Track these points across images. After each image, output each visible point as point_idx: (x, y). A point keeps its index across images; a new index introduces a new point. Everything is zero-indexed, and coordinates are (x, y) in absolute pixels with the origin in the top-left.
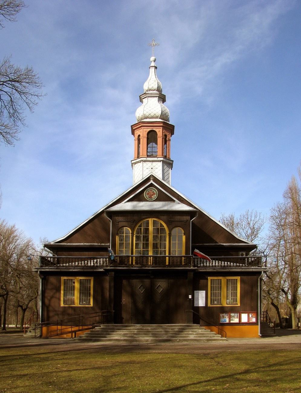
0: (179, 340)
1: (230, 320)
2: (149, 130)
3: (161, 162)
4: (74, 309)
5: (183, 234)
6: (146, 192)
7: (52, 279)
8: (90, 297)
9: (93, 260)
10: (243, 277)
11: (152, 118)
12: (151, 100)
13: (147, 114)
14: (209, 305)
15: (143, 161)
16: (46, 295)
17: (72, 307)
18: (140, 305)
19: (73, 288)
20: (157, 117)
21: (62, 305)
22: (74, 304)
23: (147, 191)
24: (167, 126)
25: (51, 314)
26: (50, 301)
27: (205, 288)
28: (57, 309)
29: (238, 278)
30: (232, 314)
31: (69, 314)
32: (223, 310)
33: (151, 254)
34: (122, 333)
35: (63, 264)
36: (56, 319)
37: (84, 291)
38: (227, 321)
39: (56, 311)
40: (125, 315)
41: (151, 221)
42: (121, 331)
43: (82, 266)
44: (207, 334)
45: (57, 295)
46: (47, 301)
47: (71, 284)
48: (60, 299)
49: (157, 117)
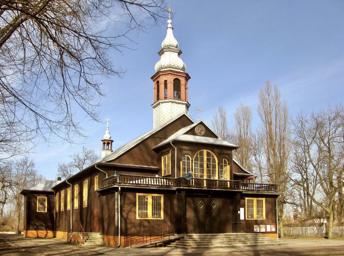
0: (261, 245)
1: (260, 230)
2: (175, 78)
3: (185, 105)
4: (148, 221)
5: (228, 164)
6: (197, 128)
7: (130, 195)
8: (160, 211)
9: (145, 179)
10: (267, 198)
11: (166, 68)
12: (172, 54)
13: (172, 65)
14: (246, 219)
15: (171, 102)
16: (124, 209)
17: (146, 220)
18: (202, 219)
19: (146, 204)
20: (179, 69)
21: (138, 218)
22: (148, 217)
23: (197, 127)
24: (187, 78)
25: (129, 226)
26: (127, 214)
27: (244, 206)
28: (133, 221)
29: (264, 199)
30: (261, 226)
31: (144, 226)
32: (257, 223)
33: (205, 177)
34: (218, 241)
35: (130, 181)
36: (133, 230)
37: (156, 207)
38: (258, 231)
39: (133, 223)
40: (190, 227)
41: (205, 151)
42: (214, 239)
43: (159, 185)
44: (274, 240)
45: (133, 209)
46: (124, 214)
47: (145, 200)
48: (135, 213)
49: (179, 69)
